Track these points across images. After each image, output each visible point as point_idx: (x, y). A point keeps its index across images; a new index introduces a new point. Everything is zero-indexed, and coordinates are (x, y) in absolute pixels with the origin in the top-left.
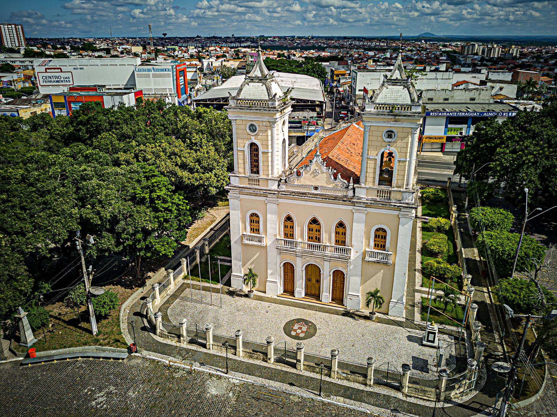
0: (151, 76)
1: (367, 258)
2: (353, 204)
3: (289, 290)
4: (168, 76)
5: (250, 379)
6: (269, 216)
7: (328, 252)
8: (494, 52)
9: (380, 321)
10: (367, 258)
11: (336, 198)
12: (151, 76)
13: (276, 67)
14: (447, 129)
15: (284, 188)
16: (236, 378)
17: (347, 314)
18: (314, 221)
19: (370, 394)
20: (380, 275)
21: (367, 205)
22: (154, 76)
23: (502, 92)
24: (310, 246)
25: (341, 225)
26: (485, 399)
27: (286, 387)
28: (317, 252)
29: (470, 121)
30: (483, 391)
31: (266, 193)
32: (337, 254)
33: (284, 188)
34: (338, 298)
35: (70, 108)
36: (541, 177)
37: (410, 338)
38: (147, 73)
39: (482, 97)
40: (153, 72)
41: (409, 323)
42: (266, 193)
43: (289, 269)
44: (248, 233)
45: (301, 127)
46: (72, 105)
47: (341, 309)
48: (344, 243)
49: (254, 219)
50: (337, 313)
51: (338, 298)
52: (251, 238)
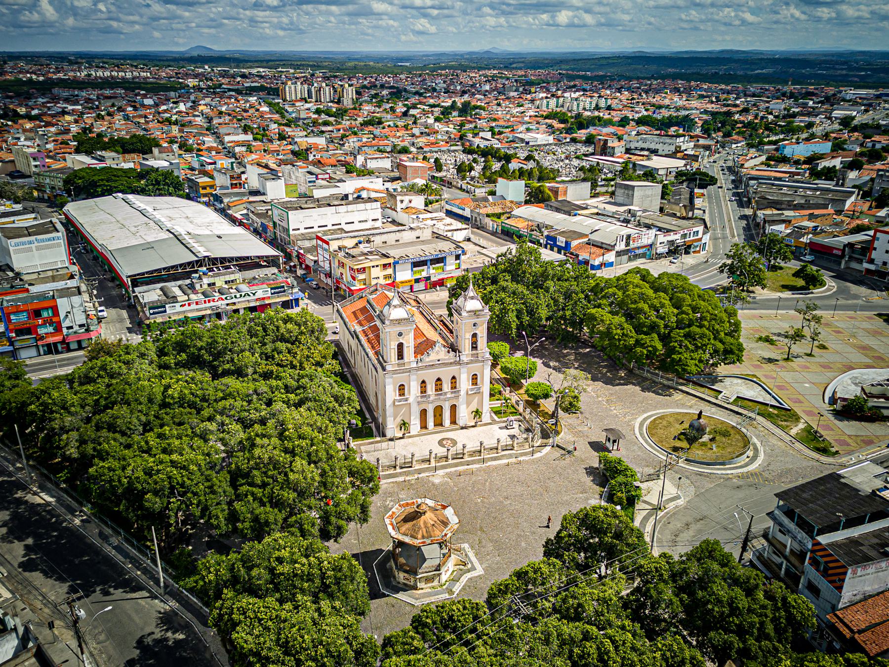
0: (34, 249)
1: (470, 393)
2: (460, 364)
3: (424, 426)
4: (59, 245)
5: (448, 470)
6: (412, 383)
7: (449, 395)
8: (325, 94)
9: (481, 425)
10: (397, 403)
11: (451, 363)
12: (34, 249)
13: (107, 181)
14: (414, 273)
15: (420, 364)
16: (441, 472)
17: (462, 428)
18: (439, 379)
19: (502, 456)
20: (476, 400)
21: (467, 363)
22: (38, 248)
23: (412, 205)
24: (422, 397)
25: (454, 378)
26: (545, 441)
27: (466, 467)
28: (442, 397)
29: (429, 263)
30: (543, 438)
31: (409, 371)
32: (453, 395)
33: (420, 364)
34: (453, 422)
35: (10, 320)
36: (517, 317)
37: (500, 428)
38: (27, 246)
39: (425, 234)
40: (36, 244)
41: (494, 422)
42: (409, 371)
43: (424, 413)
44: (398, 398)
45: (284, 291)
46: (12, 317)
47: (457, 427)
48: (455, 388)
49: (402, 388)
50: (457, 429)
51: (453, 422)
52: (400, 401)
